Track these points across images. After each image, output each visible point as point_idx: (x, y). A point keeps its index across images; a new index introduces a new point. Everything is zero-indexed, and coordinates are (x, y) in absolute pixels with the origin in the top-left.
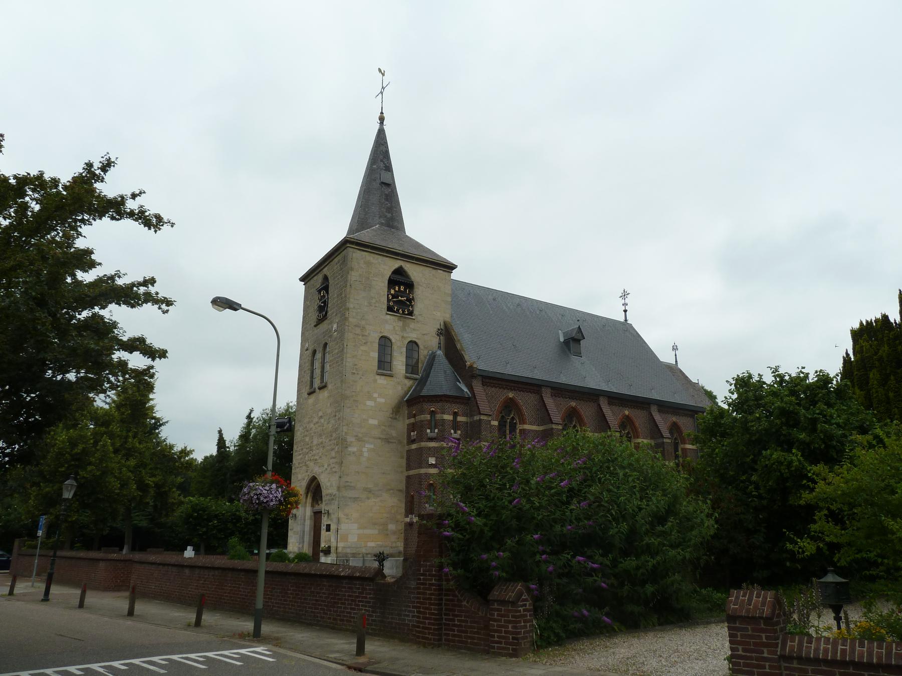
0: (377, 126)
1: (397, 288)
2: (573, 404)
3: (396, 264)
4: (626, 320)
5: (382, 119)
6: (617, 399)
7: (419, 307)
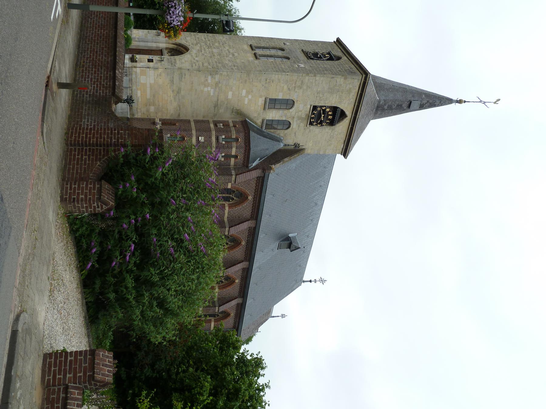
0: (455, 98)
1: (330, 113)
2: (243, 243)
3: (349, 113)
4: (304, 282)
5: (460, 102)
6: (246, 275)
7: (316, 130)
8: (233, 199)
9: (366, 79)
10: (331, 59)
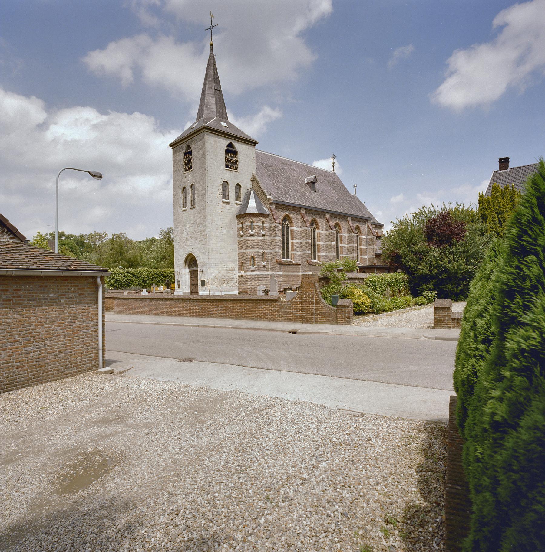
2: (314, 217)
7: (240, 165)
8: (287, 224)
9: (207, 129)
10: (190, 153)
